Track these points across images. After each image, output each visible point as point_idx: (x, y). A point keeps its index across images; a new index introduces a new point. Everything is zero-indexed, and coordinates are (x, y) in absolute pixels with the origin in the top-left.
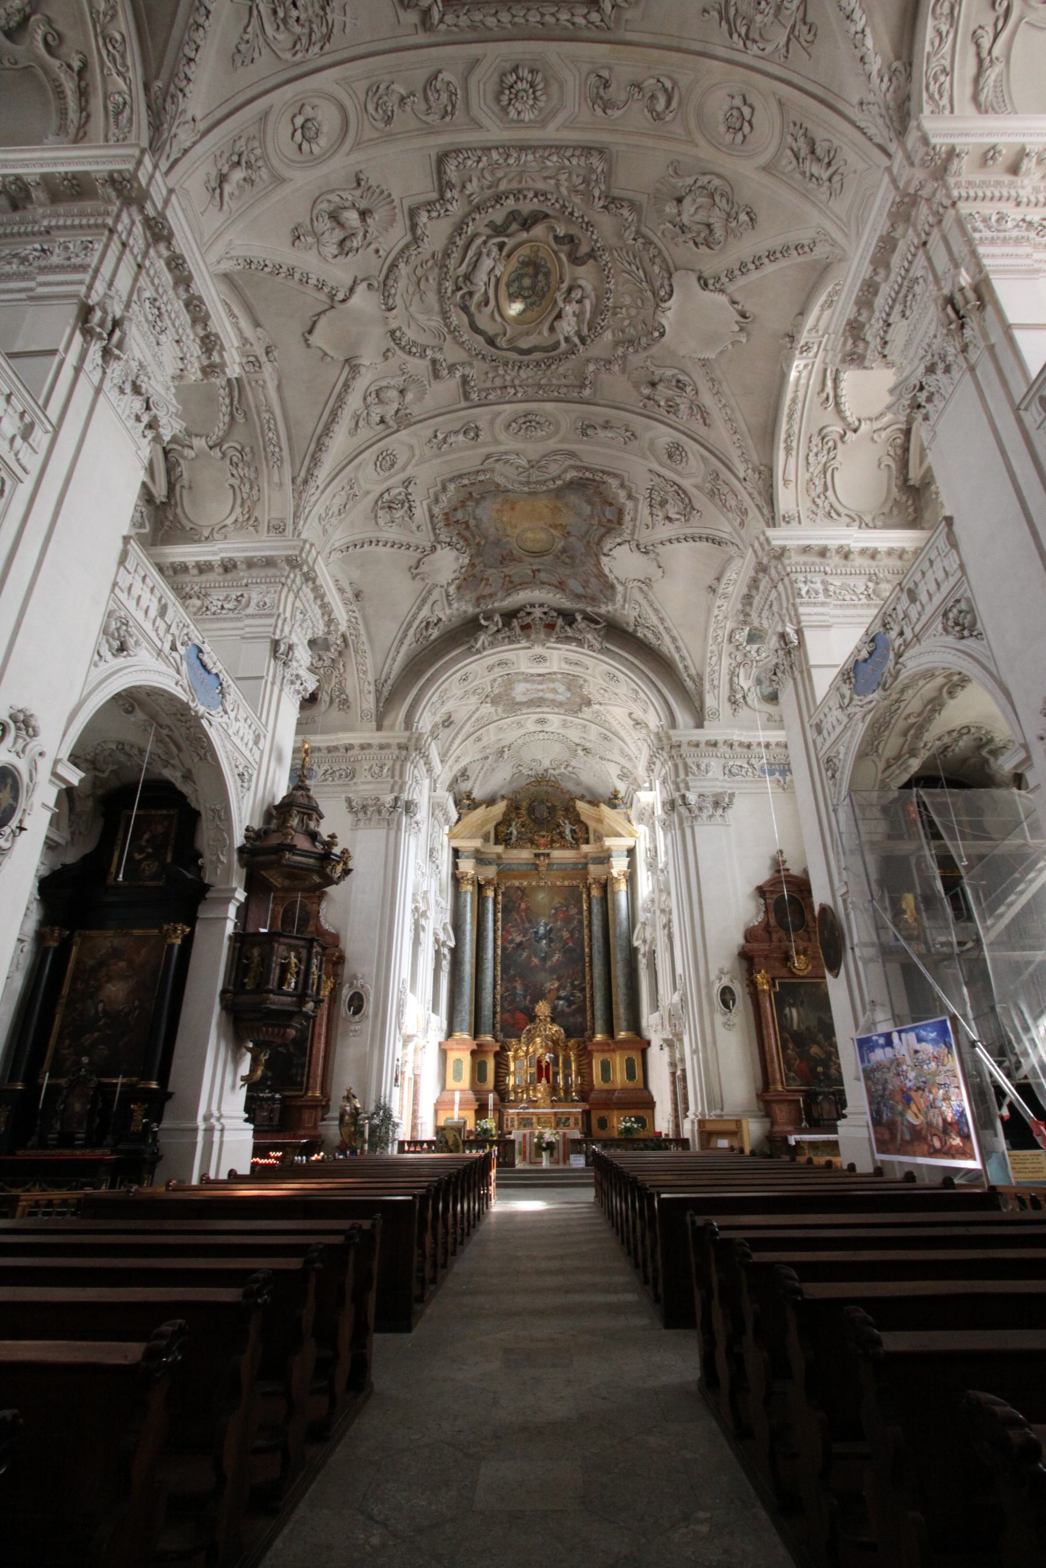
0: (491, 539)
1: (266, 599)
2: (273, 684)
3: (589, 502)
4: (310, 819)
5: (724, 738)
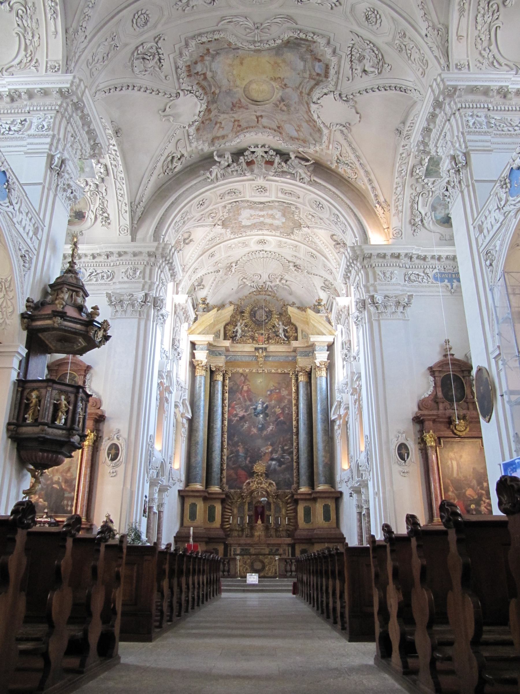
0: (224, 89)
1: (45, 124)
2: (49, 189)
3: (302, 58)
5: (406, 251)
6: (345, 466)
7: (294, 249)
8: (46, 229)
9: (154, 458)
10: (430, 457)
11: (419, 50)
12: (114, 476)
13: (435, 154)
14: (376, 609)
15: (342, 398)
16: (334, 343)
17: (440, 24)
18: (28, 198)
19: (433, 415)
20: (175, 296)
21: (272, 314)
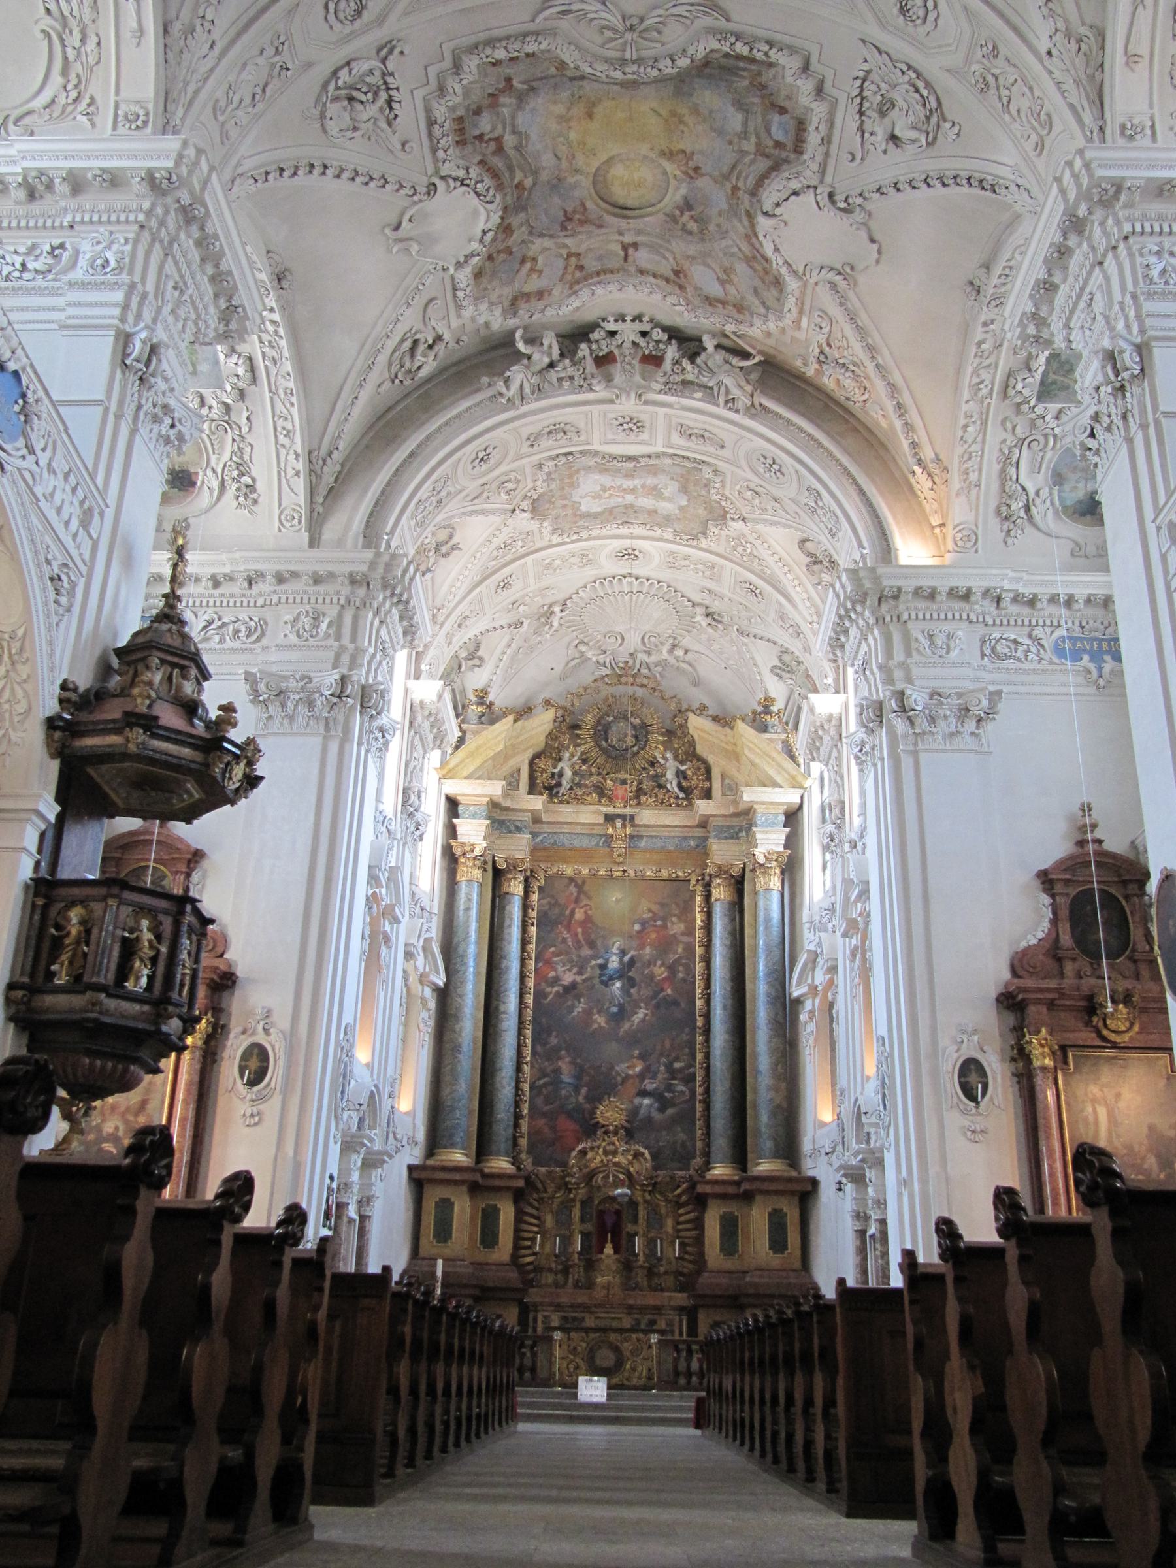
1: (110, 255)
2: (119, 417)
3: (739, 105)
4: (185, 677)
5: (986, 584)
6: (827, 1116)
7: (708, 573)
8: (109, 513)
9: (353, 1083)
10: (1039, 1096)
11: (1031, 89)
12: (256, 1124)
13: (1063, 345)
14: (917, 1425)
15: (820, 944)
16: (801, 807)
17: (1083, 24)
18: (69, 436)
19: (1048, 990)
20: (412, 683)
21: (648, 733)
